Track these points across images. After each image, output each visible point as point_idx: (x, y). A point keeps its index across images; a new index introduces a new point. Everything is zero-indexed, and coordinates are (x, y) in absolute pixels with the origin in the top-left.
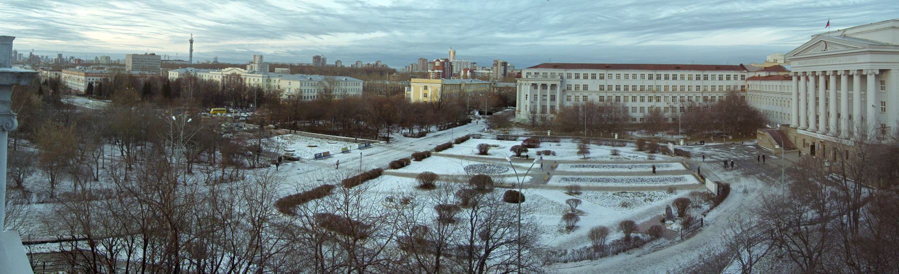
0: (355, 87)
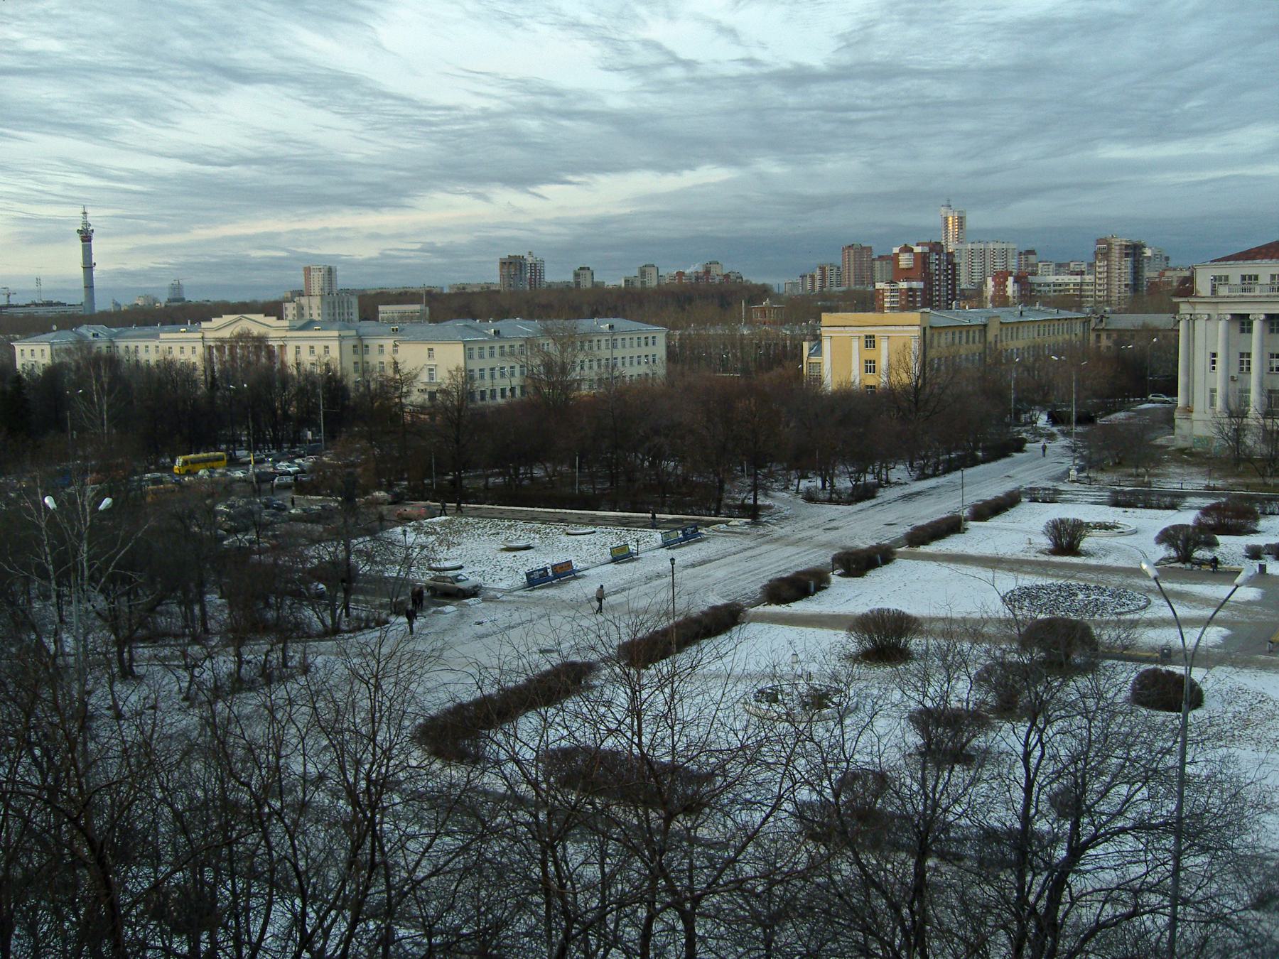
0: (644, 351)
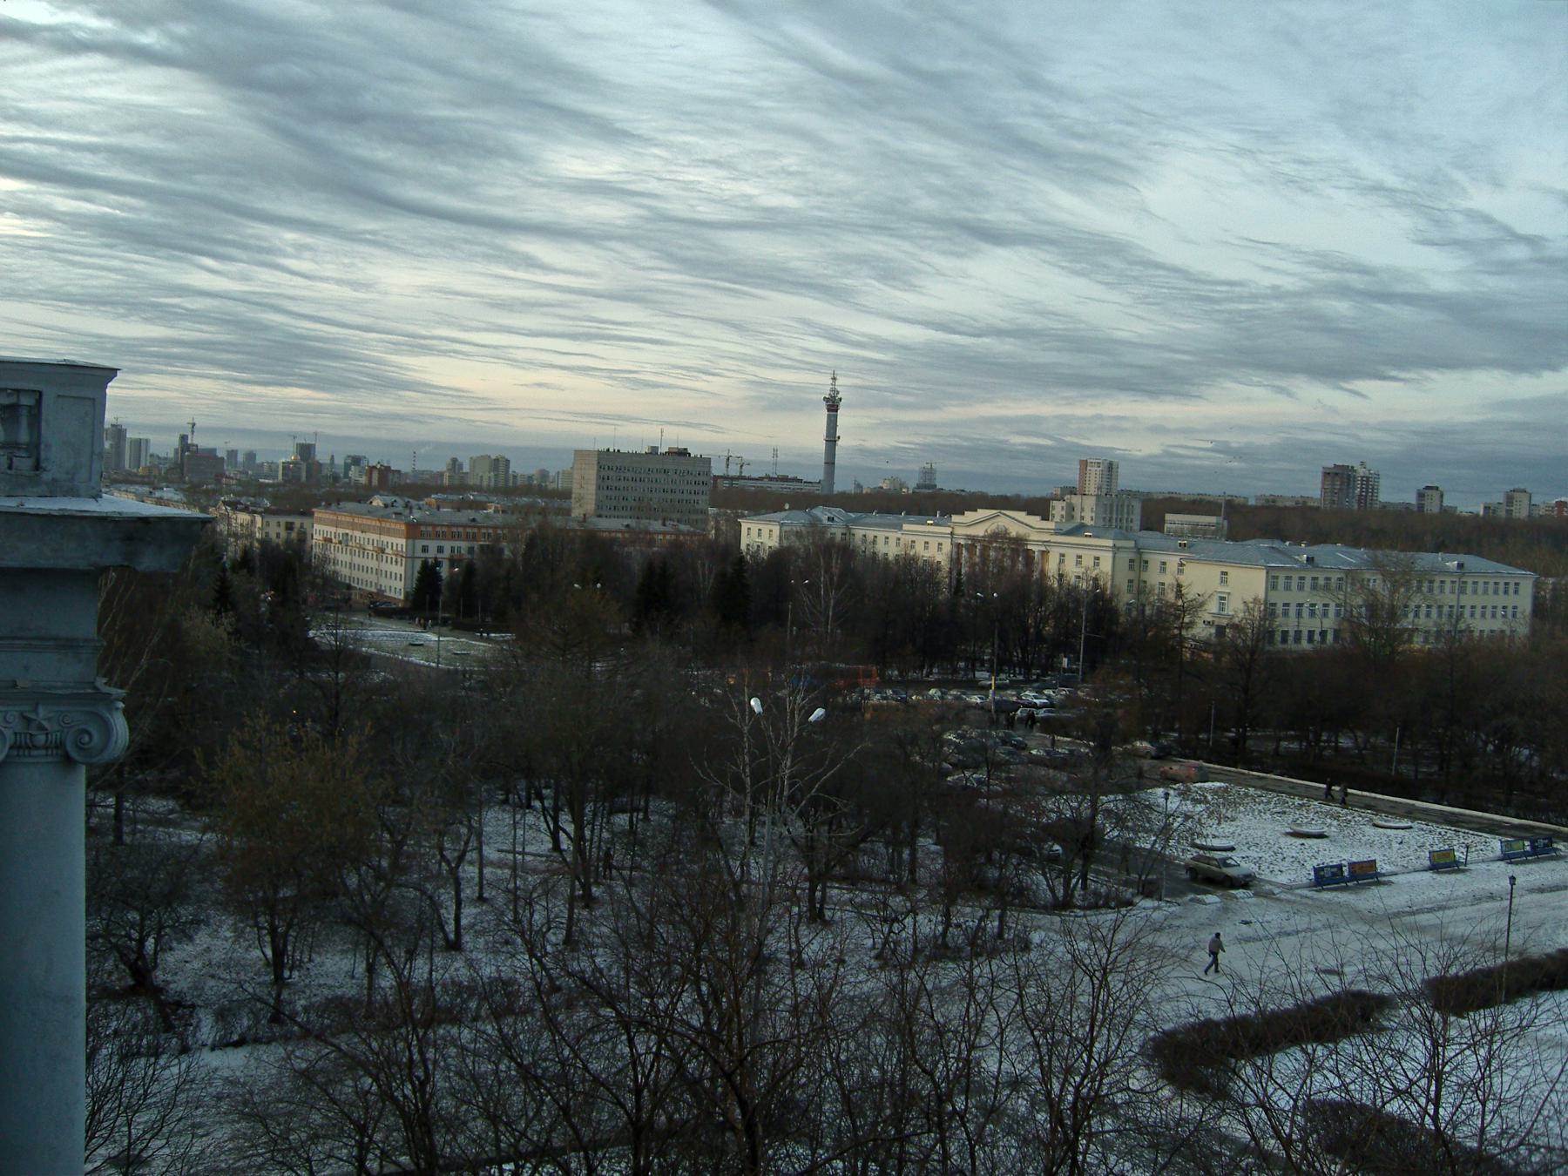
0: (1501, 600)
